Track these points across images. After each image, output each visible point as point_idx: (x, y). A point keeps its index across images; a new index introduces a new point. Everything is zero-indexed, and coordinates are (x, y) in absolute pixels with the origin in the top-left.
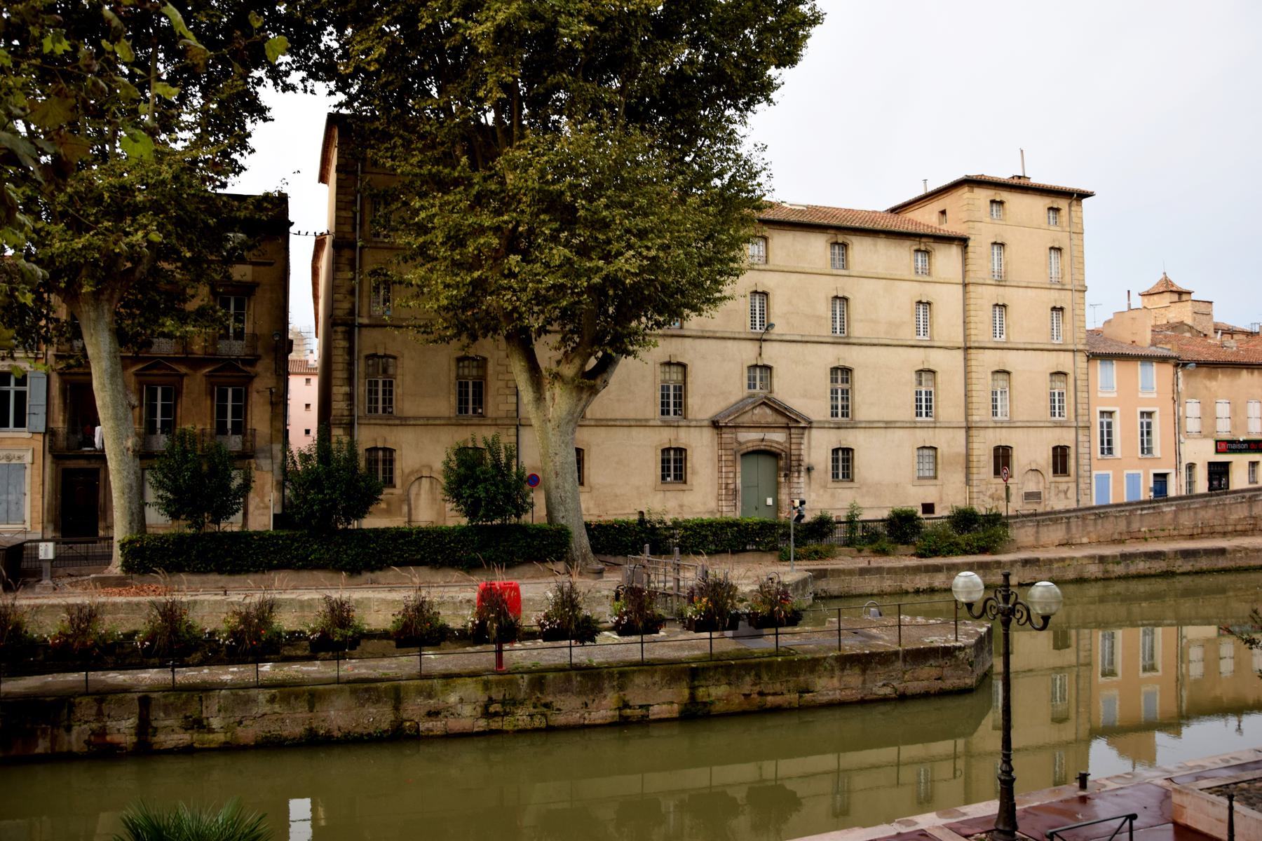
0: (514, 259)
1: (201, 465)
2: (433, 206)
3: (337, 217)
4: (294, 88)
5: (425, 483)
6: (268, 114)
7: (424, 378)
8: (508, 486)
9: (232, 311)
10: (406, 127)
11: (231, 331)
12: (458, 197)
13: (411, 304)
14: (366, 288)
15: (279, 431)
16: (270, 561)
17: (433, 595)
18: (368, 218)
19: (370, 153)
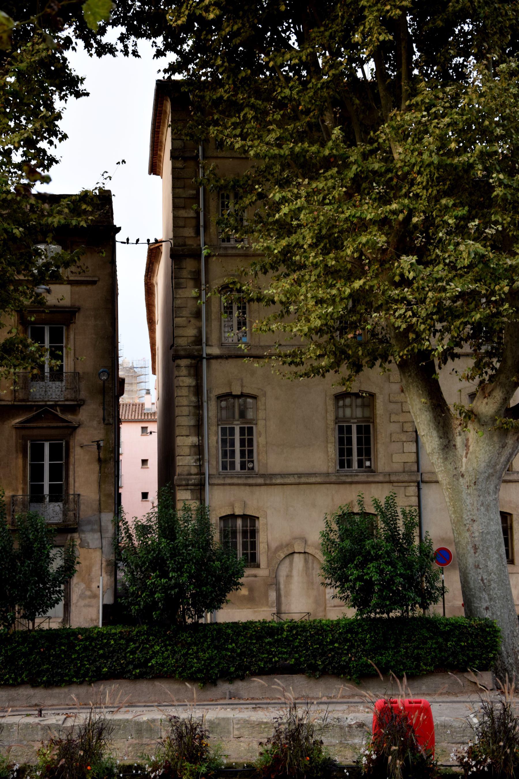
0: (407, 261)
1: (11, 542)
2: (298, 197)
3: (175, 218)
4: (111, 50)
5: (298, 561)
6: (81, 87)
7: (294, 421)
8: (409, 566)
9: (47, 344)
10: (258, 93)
11: (47, 369)
12: (330, 183)
13: (274, 327)
14: (215, 308)
15: (108, 496)
16: (99, 669)
17: (314, 715)
18: (213, 218)
19: (213, 131)
